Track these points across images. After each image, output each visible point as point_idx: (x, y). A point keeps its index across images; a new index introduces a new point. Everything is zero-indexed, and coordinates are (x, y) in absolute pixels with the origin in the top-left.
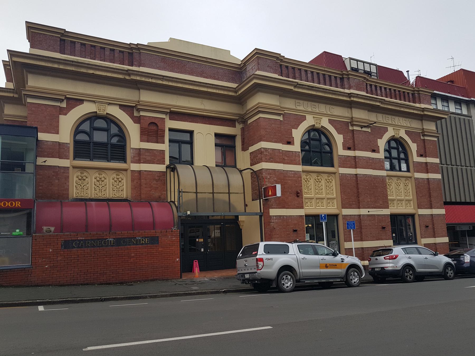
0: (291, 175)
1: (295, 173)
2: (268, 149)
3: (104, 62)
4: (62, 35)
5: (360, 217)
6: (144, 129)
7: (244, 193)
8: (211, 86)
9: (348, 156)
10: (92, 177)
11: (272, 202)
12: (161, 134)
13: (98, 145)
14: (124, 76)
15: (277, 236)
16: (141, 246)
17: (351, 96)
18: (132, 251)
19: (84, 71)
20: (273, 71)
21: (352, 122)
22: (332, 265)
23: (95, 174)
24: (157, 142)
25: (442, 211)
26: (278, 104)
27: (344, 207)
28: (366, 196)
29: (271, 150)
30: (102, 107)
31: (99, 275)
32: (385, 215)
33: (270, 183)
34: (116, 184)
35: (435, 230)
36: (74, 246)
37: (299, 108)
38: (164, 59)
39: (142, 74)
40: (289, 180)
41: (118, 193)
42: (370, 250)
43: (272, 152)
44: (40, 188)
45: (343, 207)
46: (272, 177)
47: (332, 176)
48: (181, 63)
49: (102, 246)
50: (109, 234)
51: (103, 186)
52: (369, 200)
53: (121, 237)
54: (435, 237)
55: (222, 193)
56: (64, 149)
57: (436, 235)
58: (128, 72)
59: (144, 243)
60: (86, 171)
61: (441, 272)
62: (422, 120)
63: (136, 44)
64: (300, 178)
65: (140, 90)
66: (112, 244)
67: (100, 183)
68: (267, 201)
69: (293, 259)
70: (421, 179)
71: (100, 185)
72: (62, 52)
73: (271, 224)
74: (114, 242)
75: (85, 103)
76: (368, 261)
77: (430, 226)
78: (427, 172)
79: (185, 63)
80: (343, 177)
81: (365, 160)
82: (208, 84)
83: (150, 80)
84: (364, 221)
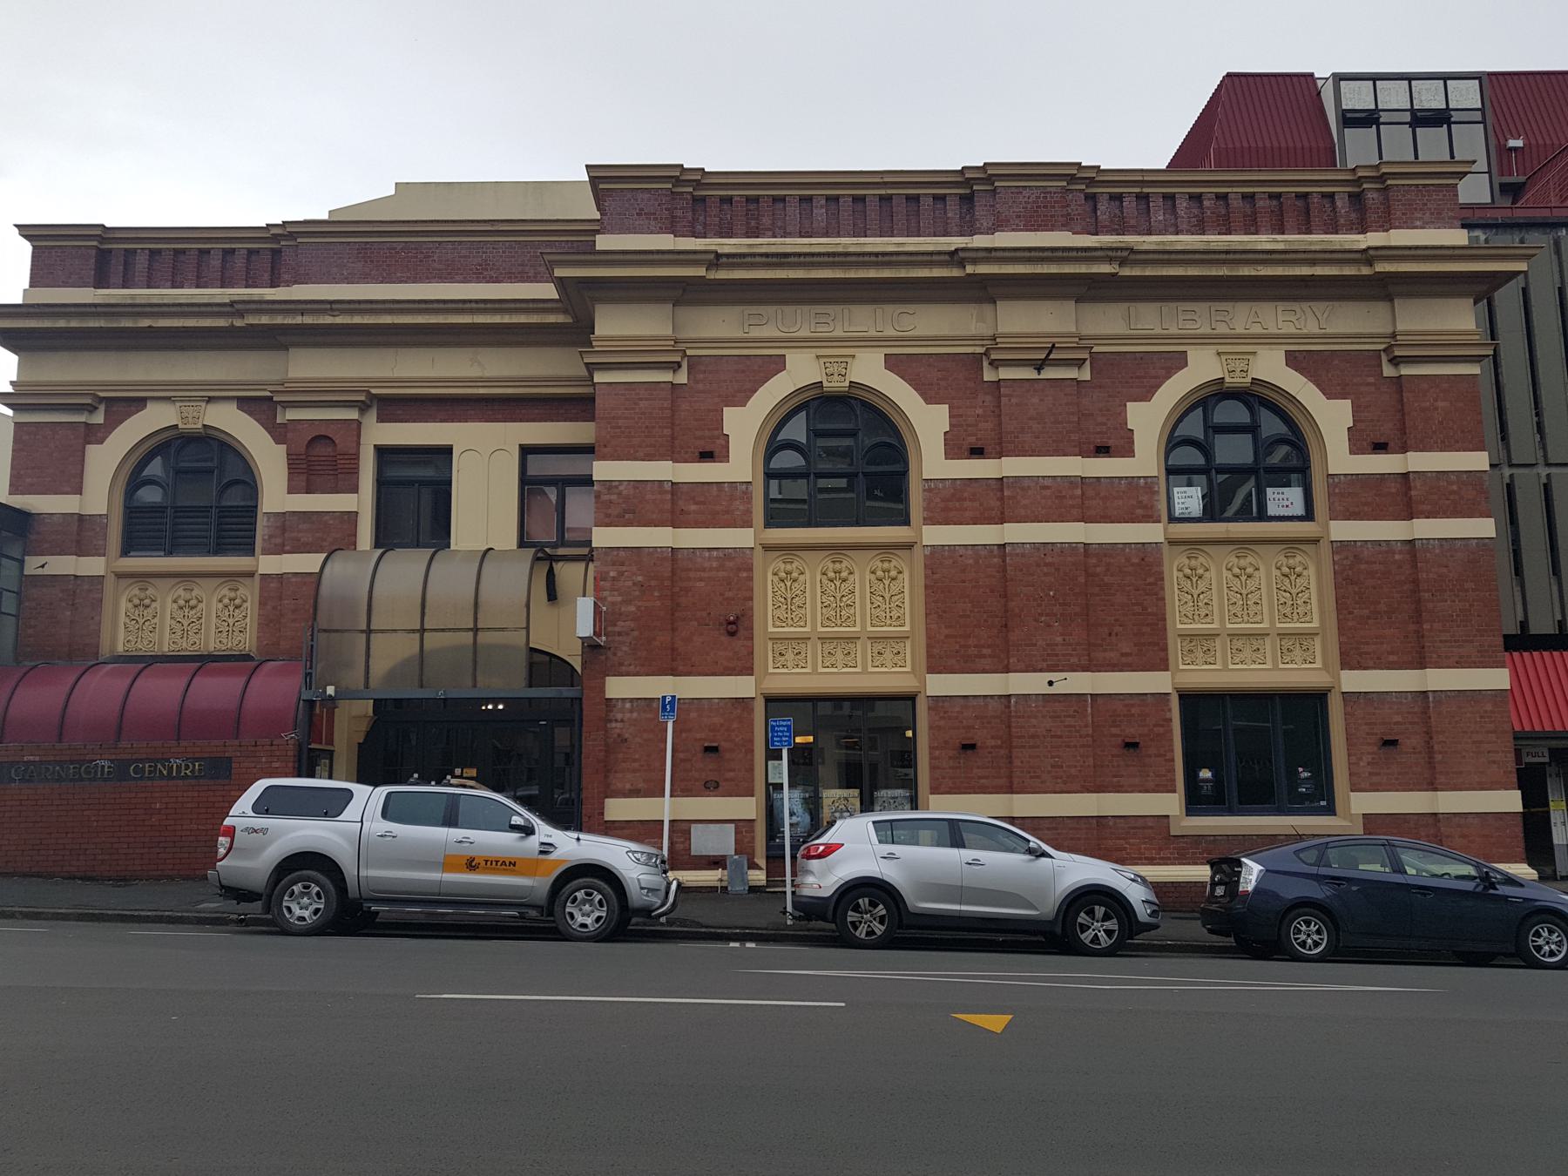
0: (707, 565)
1: (727, 554)
2: (617, 483)
3: (916, 238)
4: (101, 239)
5: (1010, 702)
6: (294, 457)
7: (527, 628)
8: (482, 306)
9: (967, 482)
10: (167, 601)
11: (619, 654)
12: (347, 466)
13: (186, 511)
14: (230, 320)
15: (633, 764)
16: (180, 782)
17: (963, 259)
18: (157, 795)
19: (127, 325)
20: (660, 225)
21: (992, 350)
22: (494, 863)
23: (130, 588)
24: (335, 490)
25: (1497, 679)
26: (669, 332)
27: (936, 665)
28: (1042, 624)
29: (629, 484)
30: (190, 411)
31: (68, 853)
32: (1141, 697)
33: (616, 593)
34: (227, 614)
35: (1438, 757)
36: (13, 776)
37: (756, 333)
38: (366, 249)
39: (270, 306)
40: (701, 580)
41: (230, 638)
42: (1048, 829)
43: (632, 492)
44: (30, 631)
45: (932, 669)
46: (626, 573)
47: (899, 556)
48: (415, 251)
49: (82, 779)
50: (100, 748)
51: (193, 622)
52: (1059, 639)
53: (129, 757)
54: (1436, 790)
55: (450, 630)
56: (94, 530)
57: (1442, 779)
58: (955, 257)
59: (190, 774)
60: (1202, 551)
61: (1050, 921)
62: (1391, 300)
63: (960, 168)
64: (745, 570)
65: (995, 302)
66: (105, 776)
67: (186, 614)
68: (595, 651)
69: (343, 834)
70: (1369, 545)
71: (186, 617)
72: (101, 282)
73: (614, 725)
74: (112, 770)
75: (150, 405)
76: (1208, 867)
77: (1412, 741)
78: (1409, 514)
79: (430, 249)
80: (938, 558)
81: (1047, 488)
82: (470, 301)
83: (299, 320)
84: (1023, 717)
